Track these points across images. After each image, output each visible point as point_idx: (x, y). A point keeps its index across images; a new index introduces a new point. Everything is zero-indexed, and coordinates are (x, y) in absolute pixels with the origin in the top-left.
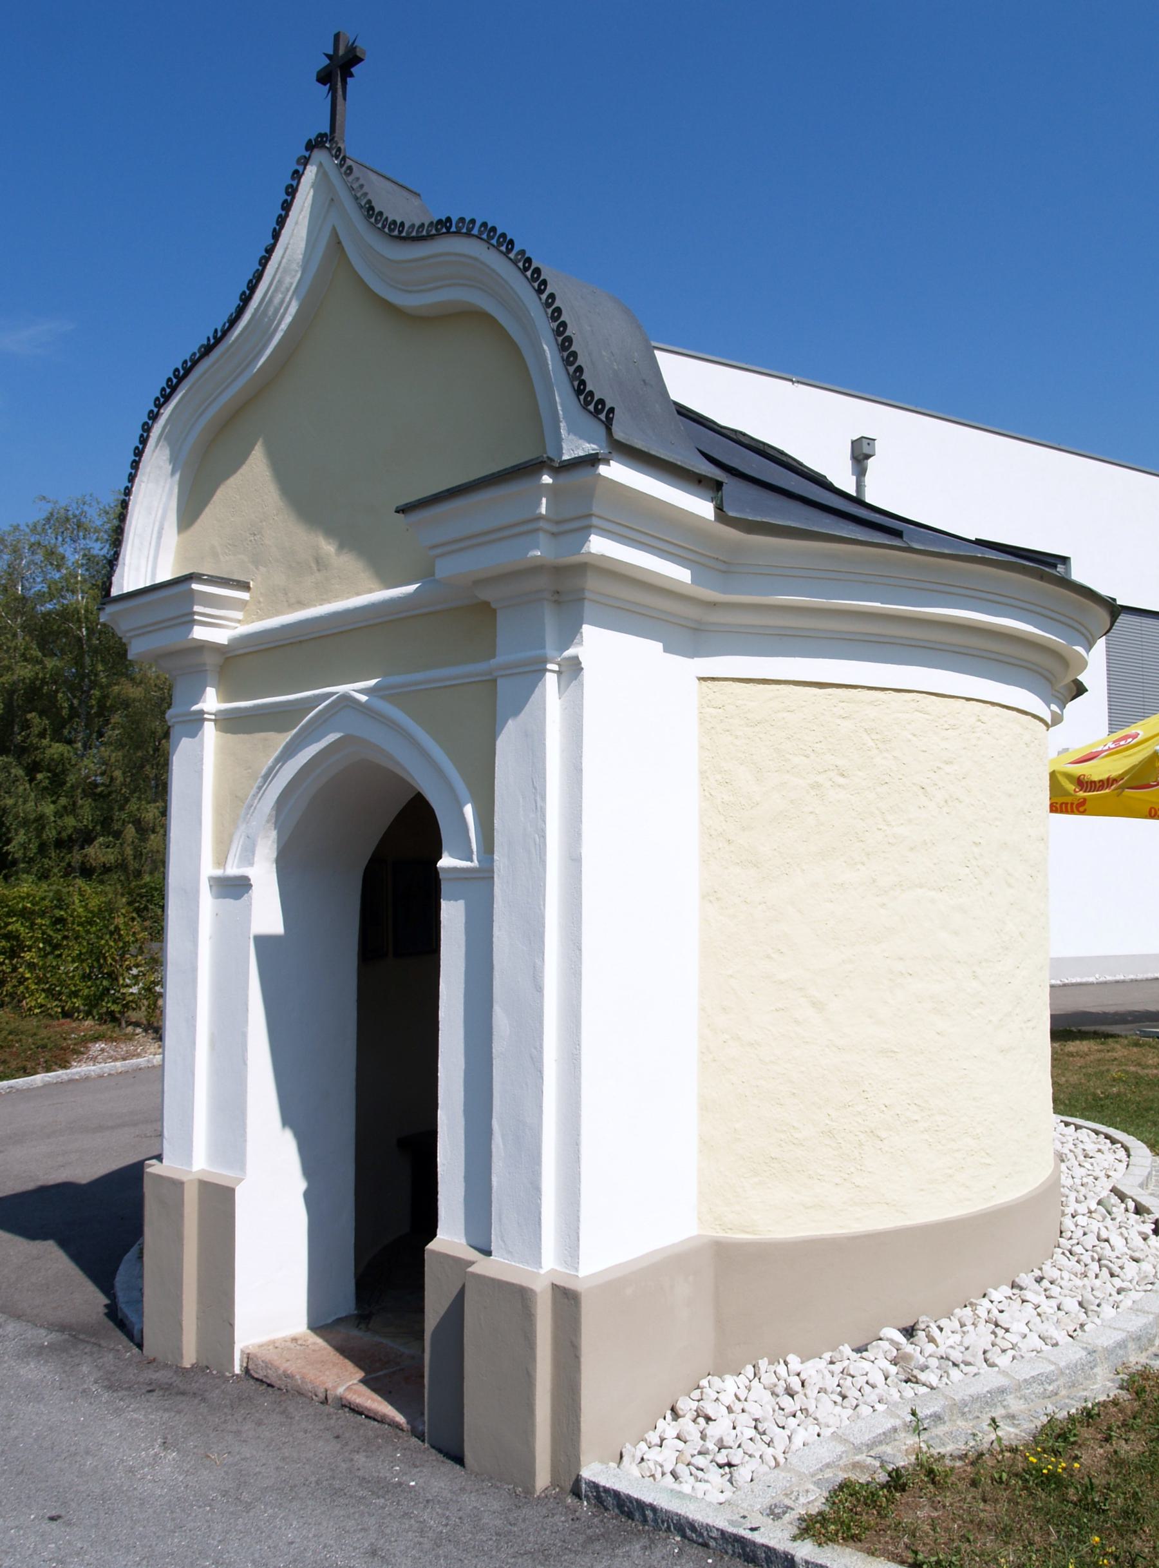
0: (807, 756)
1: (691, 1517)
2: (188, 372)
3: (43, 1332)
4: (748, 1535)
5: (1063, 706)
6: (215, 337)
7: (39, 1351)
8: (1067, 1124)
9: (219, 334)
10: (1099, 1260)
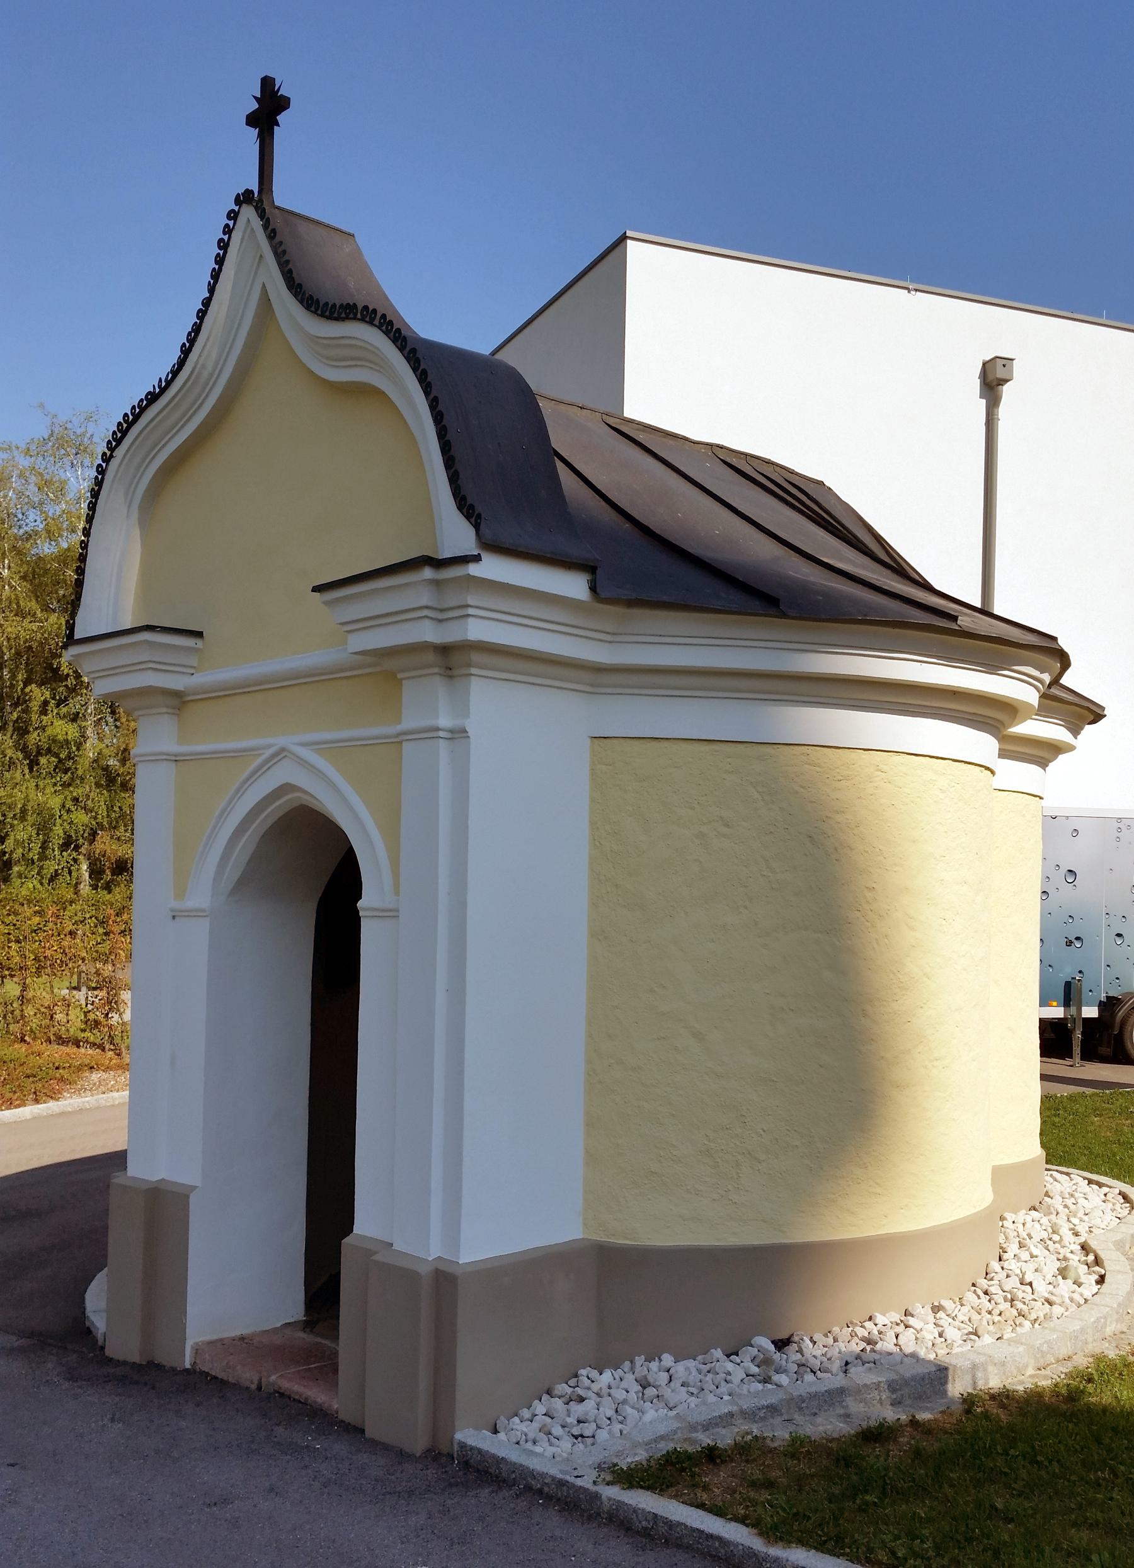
0: (693, 808)
1: (531, 1467)
2: (137, 417)
3: (14, 1338)
4: (572, 1480)
5: (1076, 731)
6: (160, 386)
7: (11, 1352)
8: (1090, 1182)
9: (164, 384)
10: (1012, 1300)
